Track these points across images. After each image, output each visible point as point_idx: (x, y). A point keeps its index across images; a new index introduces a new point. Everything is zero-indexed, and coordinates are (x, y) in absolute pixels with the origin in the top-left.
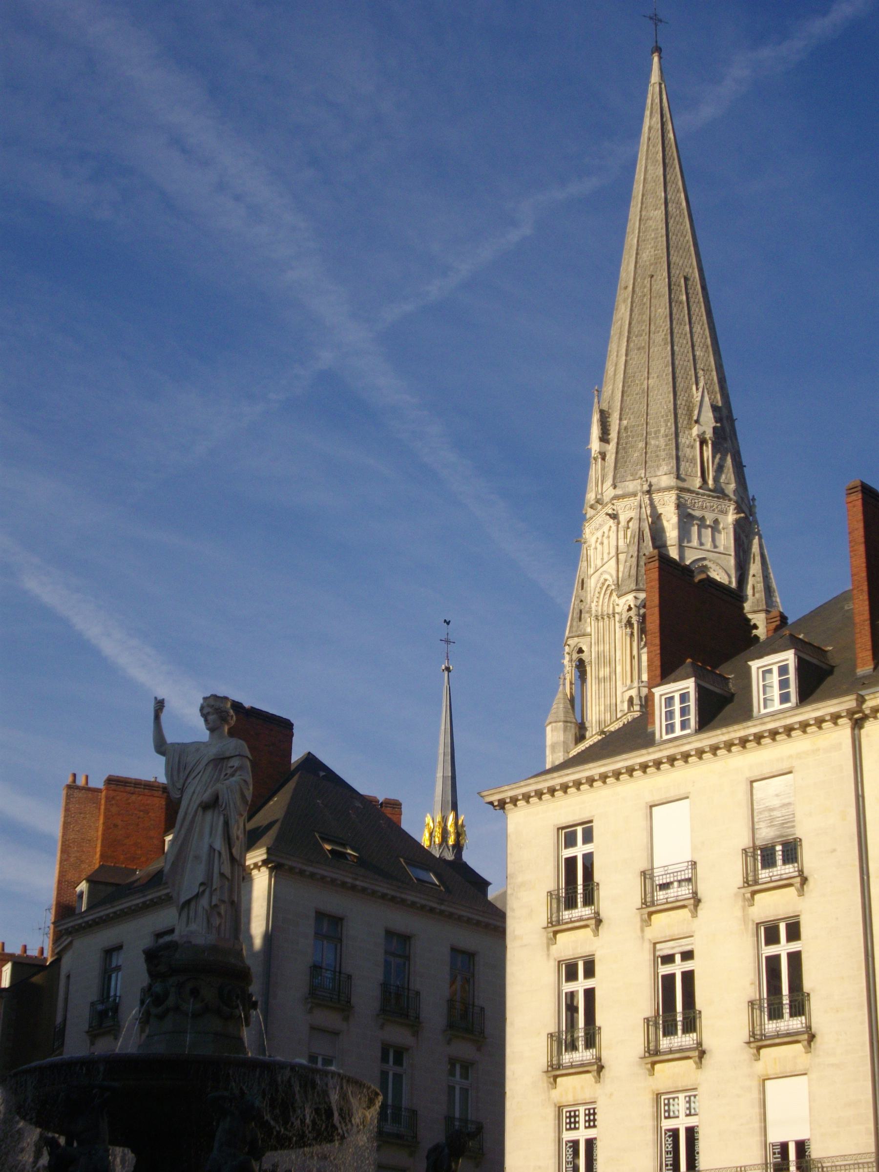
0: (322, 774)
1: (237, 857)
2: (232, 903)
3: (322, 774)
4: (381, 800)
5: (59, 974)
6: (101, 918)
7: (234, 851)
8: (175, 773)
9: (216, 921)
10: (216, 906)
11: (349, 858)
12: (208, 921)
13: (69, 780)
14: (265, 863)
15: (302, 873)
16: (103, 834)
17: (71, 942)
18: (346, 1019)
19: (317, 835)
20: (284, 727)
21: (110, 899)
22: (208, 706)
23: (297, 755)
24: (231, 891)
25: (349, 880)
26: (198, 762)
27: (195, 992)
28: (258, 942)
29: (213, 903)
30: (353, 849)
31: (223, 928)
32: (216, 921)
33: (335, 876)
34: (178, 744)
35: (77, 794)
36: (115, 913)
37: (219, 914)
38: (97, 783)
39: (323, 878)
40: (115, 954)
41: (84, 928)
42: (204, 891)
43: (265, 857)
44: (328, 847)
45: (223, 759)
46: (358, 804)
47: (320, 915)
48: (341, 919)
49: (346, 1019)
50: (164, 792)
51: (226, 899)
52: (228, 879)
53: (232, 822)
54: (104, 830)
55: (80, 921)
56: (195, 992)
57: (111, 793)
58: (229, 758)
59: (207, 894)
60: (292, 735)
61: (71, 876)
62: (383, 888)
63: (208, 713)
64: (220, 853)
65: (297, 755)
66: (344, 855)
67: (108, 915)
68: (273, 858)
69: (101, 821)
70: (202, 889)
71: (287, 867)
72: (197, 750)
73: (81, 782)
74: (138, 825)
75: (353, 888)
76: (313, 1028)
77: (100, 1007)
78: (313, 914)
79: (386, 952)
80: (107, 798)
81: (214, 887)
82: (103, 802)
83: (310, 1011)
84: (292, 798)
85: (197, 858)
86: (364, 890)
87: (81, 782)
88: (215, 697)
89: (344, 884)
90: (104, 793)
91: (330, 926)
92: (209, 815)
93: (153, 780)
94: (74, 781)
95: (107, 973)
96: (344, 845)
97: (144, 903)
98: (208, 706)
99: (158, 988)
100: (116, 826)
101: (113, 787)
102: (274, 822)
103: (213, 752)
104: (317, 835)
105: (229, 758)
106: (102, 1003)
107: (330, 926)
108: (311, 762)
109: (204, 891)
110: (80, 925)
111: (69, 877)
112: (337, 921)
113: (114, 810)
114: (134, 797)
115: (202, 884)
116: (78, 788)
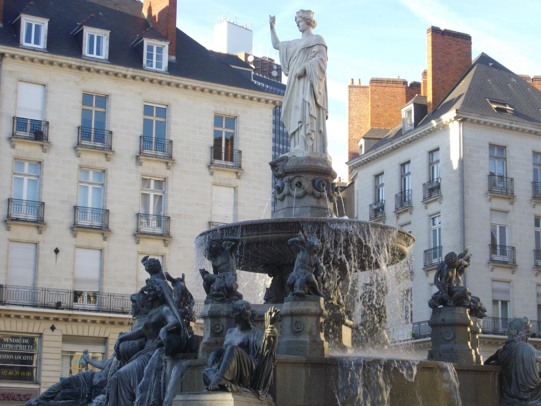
0: (491, 64)
1: (322, 105)
2: (320, 132)
3: (491, 64)
4: (532, 77)
5: (354, 191)
6: (370, 158)
7: (318, 101)
8: (285, 59)
9: (310, 143)
10: (309, 134)
11: (508, 111)
12: (305, 143)
13: (350, 83)
14: (456, 118)
15: (478, 122)
16: (371, 111)
17: (357, 174)
18: (512, 203)
19: (488, 100)
20: (466, 39)
21: (375, 147)
22: (299, 17)
23: (475, 56)
24: (319, 124)
25: (508, 124)
26: (295, 51)
27: (299, 185)
28: (455, 165)
29: (307, 133)
30: (510, 106)
31: (315, 146)
32: (310, 143)
33: (498, 122)
34: (286, 42)
35: (354, 90)
36: (377, 154)
37: (311, 139)
38: (366, 83)
39: (491, 125)
40: (380, 177)
41: (362, 164)
42: (302, 126)
43: (455, 115)
44: (494, 106)
45: (309, 47)
46: (514, 80)
47: (492, 146)
48: (505, 147)
49: (512, 203)
50: (404, 84)
51: (315, 130)
52: (315, 118)
53: (315, 85)
54: (371, 109)
55: (360, 161)
56: (299, 185)
57: (374, 88)
58: (312, 46)
59: (303, 127)
60: (471, 44)
61: (356, 136)
62: (528, 127)
63: (299, 21)
64: (309, 104)
65: (475, 56)
66: (505, 111)
67: (374, 156)
68: (460, 115)
69: (370, 104)
70: (300, 125)
71: (469, 120)
72: (295, 44)
73: (356, 83)
74: (391, 104)
75: (511, 128)
76: (492, 210)
77: (375, 207)
78: (487, 146)
79: (534, 164)
80: (371, 90)
81: (307, 123)
82: (370, 93)
83: (490, 200)
84: (472, 80)
85: (297, 107)
86: (517, 129)
87: (356, 83)
88: (303, 11)
89: (505, 127)
90: (370, 88)
91: (498, 151)
92: (302, 81)
93: (397, 78)
94: (353, 83)
95: (377, 189)
96: (505, 105)
97: (392, 147)
98: (299, 17)
99: (279, 184)
100: (378, 106)
101: (375, 84)
102: (463, 94)
103: (302, 45)
104: (488, 100)
105: (312, 46)
106: (376, 204)
107: (498, 151)
108: (484, 59)
109: (302, 126)
110: (360, 163)
111: (354, 137)
112: (502, 148)
113: (376, 97)
114: (387, 89)
115: (300, 122)
116: (355, 87)
